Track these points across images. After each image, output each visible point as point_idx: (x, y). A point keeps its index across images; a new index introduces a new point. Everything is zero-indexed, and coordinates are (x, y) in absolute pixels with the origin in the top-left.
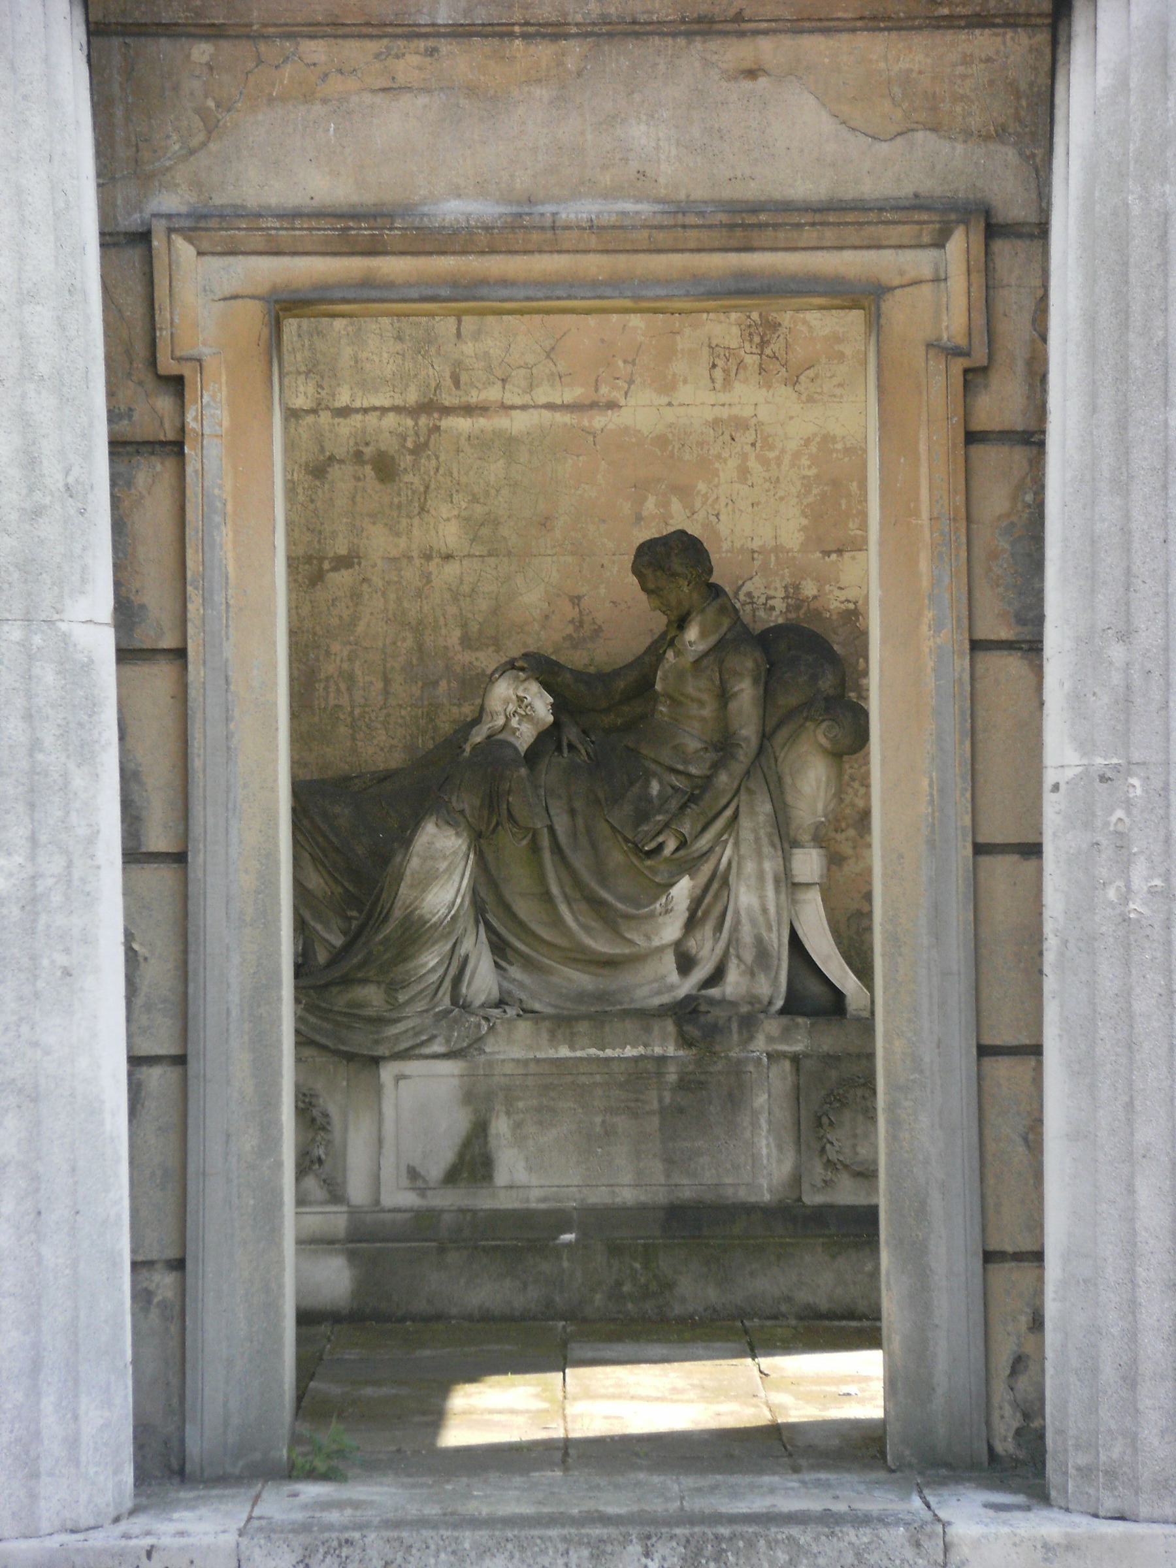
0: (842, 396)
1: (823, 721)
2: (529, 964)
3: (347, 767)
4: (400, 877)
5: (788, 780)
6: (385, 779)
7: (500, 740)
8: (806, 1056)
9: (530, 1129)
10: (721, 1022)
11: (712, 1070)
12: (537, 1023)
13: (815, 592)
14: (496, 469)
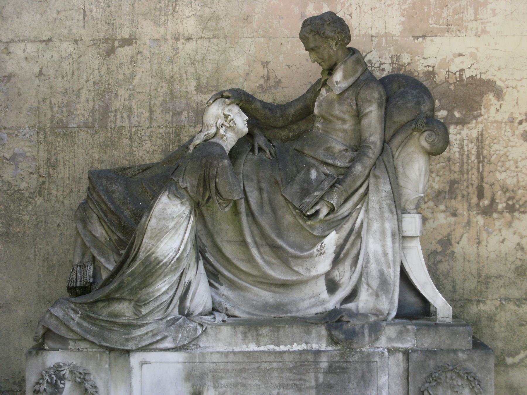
1: (425, 131)
2: (233, 285)
3: (127, 163)
4: (144, 233)
5: (400, 170)
7: (212, 142)
8: (414, 351)
10: (357, 329)
11: (350, 360)
12: (235, 328)
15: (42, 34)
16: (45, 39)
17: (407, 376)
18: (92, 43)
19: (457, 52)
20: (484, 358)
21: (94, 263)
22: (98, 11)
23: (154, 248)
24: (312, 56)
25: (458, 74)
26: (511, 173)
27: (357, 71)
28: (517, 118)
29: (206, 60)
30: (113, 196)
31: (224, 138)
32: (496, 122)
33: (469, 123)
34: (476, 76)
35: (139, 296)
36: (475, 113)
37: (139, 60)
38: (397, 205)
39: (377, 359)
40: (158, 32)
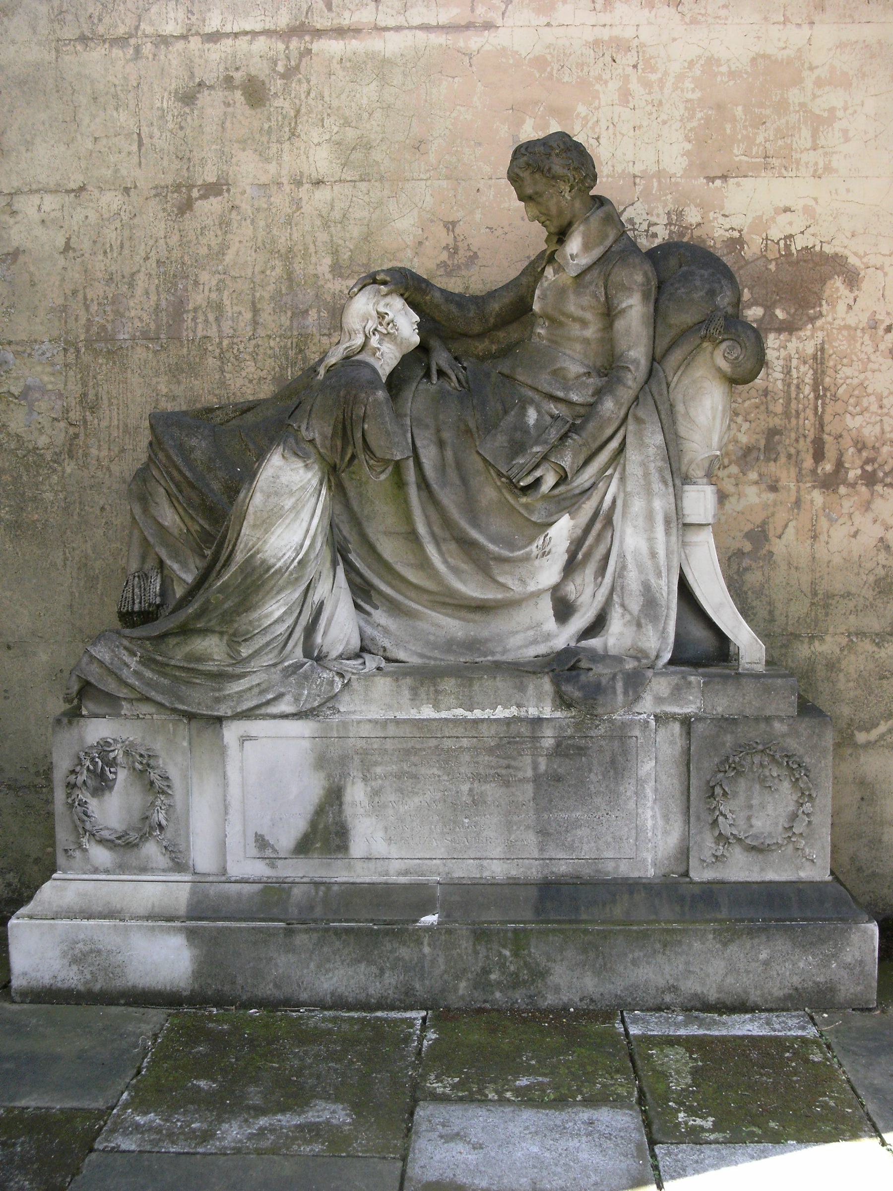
0: (726, 18)
1: (723, 340)
2: (395, 608)
3: (215, 400)
4: (242, 518)
5: (680, 408)
6: (249, 409)
8: (699, 719)
9: (390, 796)
10: (604, 681)
11: (592, 734)
12: (397, 680)
13: (698, 219)
14: (368, 92)
15: (69, 178)
16: (74, 188)
17: (687, 760)
18: (153, 192)
19: (782, 205)
20: (817, 731)
21: (162, 572)
22: (164, 137)
23: (260, 543)
24: (529, 210)
25: (782, 243)
26: (870, 418)
27: (607, 236)
28: (882, 321)
29: (348, 220)
30: (192, 456)
31: (378, 354)
32: (847, 327)
33: (801, 329)
34: (814, 246)
35: (236, 625)
36: (812, 311)
37: (233, 221)
38: (674, 470)
39: (637, 732)
40: (266, 172)
